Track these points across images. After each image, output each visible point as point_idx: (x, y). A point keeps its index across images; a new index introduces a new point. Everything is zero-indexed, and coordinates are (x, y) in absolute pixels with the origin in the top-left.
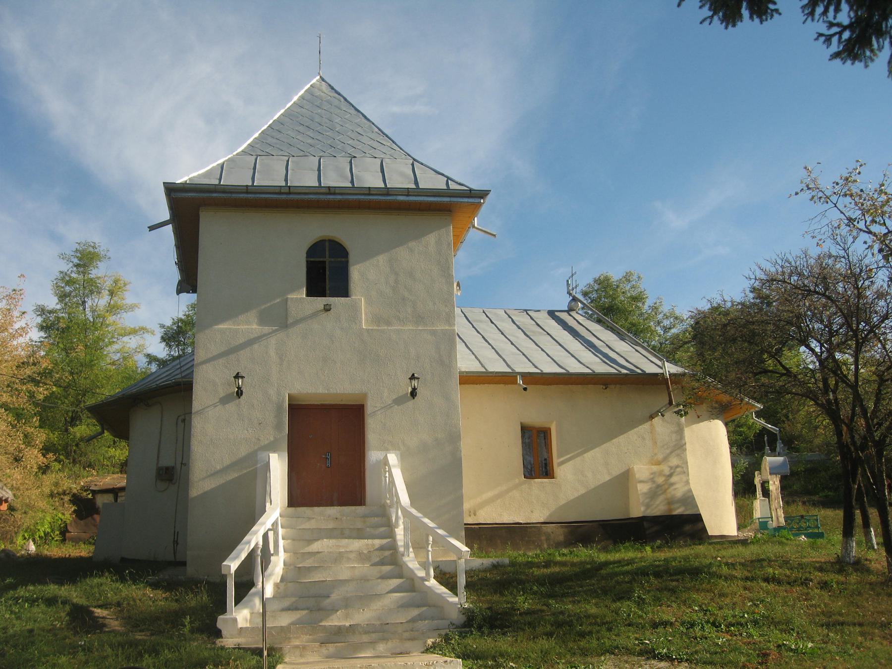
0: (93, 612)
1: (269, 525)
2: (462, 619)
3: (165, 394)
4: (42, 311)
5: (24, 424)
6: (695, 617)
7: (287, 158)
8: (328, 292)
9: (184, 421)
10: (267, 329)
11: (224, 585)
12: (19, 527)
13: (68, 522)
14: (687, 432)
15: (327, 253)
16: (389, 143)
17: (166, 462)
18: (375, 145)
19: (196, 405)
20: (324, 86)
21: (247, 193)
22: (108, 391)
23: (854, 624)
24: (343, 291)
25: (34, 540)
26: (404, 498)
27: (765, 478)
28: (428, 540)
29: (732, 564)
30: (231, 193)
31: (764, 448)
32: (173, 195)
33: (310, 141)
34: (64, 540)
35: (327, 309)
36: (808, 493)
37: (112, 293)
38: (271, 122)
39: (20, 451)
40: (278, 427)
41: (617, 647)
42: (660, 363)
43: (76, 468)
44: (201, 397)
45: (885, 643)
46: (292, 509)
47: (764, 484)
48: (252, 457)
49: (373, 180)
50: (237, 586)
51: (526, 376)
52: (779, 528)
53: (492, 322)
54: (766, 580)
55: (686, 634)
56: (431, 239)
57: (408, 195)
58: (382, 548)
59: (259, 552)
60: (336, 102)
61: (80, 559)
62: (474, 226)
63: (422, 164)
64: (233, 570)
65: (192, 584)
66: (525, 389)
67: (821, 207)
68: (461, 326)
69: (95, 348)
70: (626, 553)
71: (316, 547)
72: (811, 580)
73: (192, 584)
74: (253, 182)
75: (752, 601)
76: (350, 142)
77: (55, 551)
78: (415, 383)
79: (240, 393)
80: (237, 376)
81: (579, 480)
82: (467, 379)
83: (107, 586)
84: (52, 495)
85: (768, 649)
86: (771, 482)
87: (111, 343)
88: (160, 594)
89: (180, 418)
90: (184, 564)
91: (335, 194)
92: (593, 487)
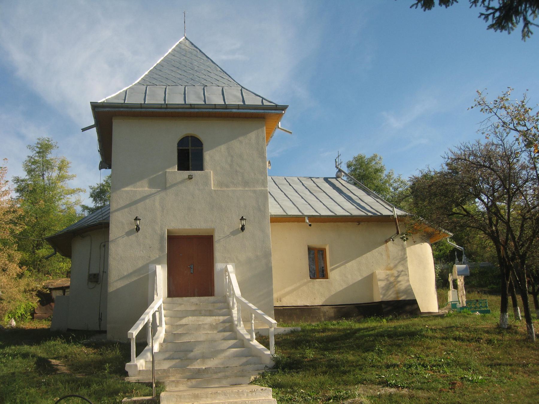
0: (51, 362)
1: (156, 308)
2: (273, 363)
3: (94, 229)
4: (17, 180)
5: (8, 249)
6: (412, 362)
7: (165, 87)
8: (191, 168)
9: (104, 246)
10: (154, 190)
11: (129, 345)
12: (5, 311)
13: (36, 308)
14: (408, 250)
15: (190, 144)
16: (227, 77)
17: (94, 271)
18: (219, 78)
19: (112, 236)
20: (187, 43)
21: (141, 108)
22: (59, 228)
23: (507, 365)
24: (200, 167)
25: (15, 319)
26: (237, 291)
27: (454, 277)
28: (252, 316)
29: (435, 330)
30: (132, 108)
31: (455, 259)
32: (96, 110)
33: (179, 76)
34: (33, 318)
35: (190, 177)
36: (481, 286)
37: (60, 169)
38: (155, 65)
39: (6, 265)
40: (161, 249)
41: (365, 380)
42: (391, 209)
43: (40, 275)
44: (114, 231)
45: (525, 375)
46: (170, 299)
47: (455, 281)
48: (145, 267)
49: (218, 100)
50: (138, 345)
51: (311, 217)
52: (463, 308)
53: (290, 185)
54: (455, 339)
55: (407, 372)
56: (253, 135)
57: (238, 109)
58: (224, 322)
59: (150, 325)
60: (195, 53)
61: (43, 329)
62: (278, 127)
63: (247, 90)
64: (134, 337)
65: (110, 344)
66: (310, 225)
67: (486, 115)
68: (271, 187)
69: (50, 201)
70: (371, 323)
71: (184, 321)
72: (481, 339)
73: (110, 344)
74: (145, 101)
75: (446, 351)
76: (203, 77)
77: (28, 325)
78: (244, 222)
79: (138, 229)
80: (136, 219)
81: (344, 279)
82: (275, 219)
83: (58, 346)
84: (25, 291)
85: (456, 380)
86: (458, 280)
87: (60, 199)
88: (91, 351)
89: (102, 244)
90: (105, 332)
91: (194, 108)
92: (351, 284)
